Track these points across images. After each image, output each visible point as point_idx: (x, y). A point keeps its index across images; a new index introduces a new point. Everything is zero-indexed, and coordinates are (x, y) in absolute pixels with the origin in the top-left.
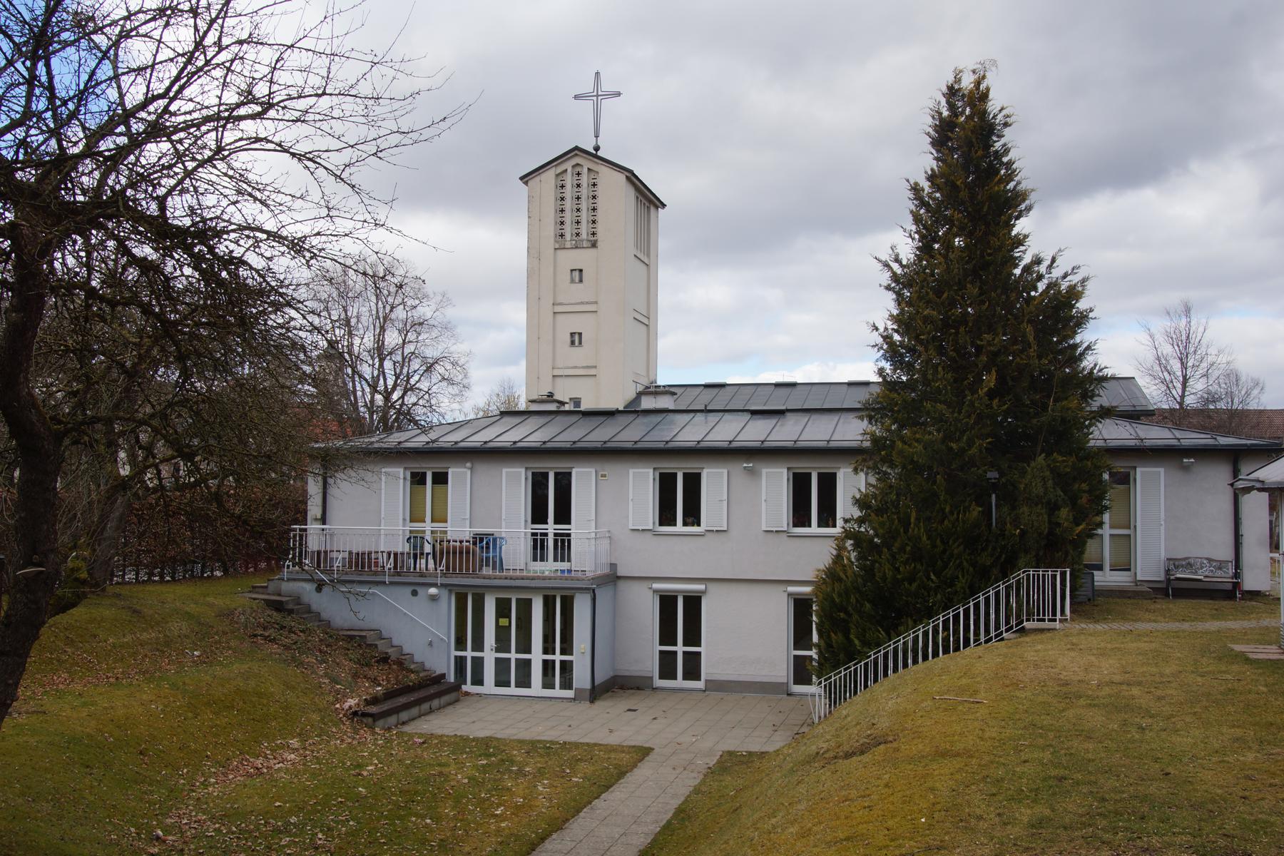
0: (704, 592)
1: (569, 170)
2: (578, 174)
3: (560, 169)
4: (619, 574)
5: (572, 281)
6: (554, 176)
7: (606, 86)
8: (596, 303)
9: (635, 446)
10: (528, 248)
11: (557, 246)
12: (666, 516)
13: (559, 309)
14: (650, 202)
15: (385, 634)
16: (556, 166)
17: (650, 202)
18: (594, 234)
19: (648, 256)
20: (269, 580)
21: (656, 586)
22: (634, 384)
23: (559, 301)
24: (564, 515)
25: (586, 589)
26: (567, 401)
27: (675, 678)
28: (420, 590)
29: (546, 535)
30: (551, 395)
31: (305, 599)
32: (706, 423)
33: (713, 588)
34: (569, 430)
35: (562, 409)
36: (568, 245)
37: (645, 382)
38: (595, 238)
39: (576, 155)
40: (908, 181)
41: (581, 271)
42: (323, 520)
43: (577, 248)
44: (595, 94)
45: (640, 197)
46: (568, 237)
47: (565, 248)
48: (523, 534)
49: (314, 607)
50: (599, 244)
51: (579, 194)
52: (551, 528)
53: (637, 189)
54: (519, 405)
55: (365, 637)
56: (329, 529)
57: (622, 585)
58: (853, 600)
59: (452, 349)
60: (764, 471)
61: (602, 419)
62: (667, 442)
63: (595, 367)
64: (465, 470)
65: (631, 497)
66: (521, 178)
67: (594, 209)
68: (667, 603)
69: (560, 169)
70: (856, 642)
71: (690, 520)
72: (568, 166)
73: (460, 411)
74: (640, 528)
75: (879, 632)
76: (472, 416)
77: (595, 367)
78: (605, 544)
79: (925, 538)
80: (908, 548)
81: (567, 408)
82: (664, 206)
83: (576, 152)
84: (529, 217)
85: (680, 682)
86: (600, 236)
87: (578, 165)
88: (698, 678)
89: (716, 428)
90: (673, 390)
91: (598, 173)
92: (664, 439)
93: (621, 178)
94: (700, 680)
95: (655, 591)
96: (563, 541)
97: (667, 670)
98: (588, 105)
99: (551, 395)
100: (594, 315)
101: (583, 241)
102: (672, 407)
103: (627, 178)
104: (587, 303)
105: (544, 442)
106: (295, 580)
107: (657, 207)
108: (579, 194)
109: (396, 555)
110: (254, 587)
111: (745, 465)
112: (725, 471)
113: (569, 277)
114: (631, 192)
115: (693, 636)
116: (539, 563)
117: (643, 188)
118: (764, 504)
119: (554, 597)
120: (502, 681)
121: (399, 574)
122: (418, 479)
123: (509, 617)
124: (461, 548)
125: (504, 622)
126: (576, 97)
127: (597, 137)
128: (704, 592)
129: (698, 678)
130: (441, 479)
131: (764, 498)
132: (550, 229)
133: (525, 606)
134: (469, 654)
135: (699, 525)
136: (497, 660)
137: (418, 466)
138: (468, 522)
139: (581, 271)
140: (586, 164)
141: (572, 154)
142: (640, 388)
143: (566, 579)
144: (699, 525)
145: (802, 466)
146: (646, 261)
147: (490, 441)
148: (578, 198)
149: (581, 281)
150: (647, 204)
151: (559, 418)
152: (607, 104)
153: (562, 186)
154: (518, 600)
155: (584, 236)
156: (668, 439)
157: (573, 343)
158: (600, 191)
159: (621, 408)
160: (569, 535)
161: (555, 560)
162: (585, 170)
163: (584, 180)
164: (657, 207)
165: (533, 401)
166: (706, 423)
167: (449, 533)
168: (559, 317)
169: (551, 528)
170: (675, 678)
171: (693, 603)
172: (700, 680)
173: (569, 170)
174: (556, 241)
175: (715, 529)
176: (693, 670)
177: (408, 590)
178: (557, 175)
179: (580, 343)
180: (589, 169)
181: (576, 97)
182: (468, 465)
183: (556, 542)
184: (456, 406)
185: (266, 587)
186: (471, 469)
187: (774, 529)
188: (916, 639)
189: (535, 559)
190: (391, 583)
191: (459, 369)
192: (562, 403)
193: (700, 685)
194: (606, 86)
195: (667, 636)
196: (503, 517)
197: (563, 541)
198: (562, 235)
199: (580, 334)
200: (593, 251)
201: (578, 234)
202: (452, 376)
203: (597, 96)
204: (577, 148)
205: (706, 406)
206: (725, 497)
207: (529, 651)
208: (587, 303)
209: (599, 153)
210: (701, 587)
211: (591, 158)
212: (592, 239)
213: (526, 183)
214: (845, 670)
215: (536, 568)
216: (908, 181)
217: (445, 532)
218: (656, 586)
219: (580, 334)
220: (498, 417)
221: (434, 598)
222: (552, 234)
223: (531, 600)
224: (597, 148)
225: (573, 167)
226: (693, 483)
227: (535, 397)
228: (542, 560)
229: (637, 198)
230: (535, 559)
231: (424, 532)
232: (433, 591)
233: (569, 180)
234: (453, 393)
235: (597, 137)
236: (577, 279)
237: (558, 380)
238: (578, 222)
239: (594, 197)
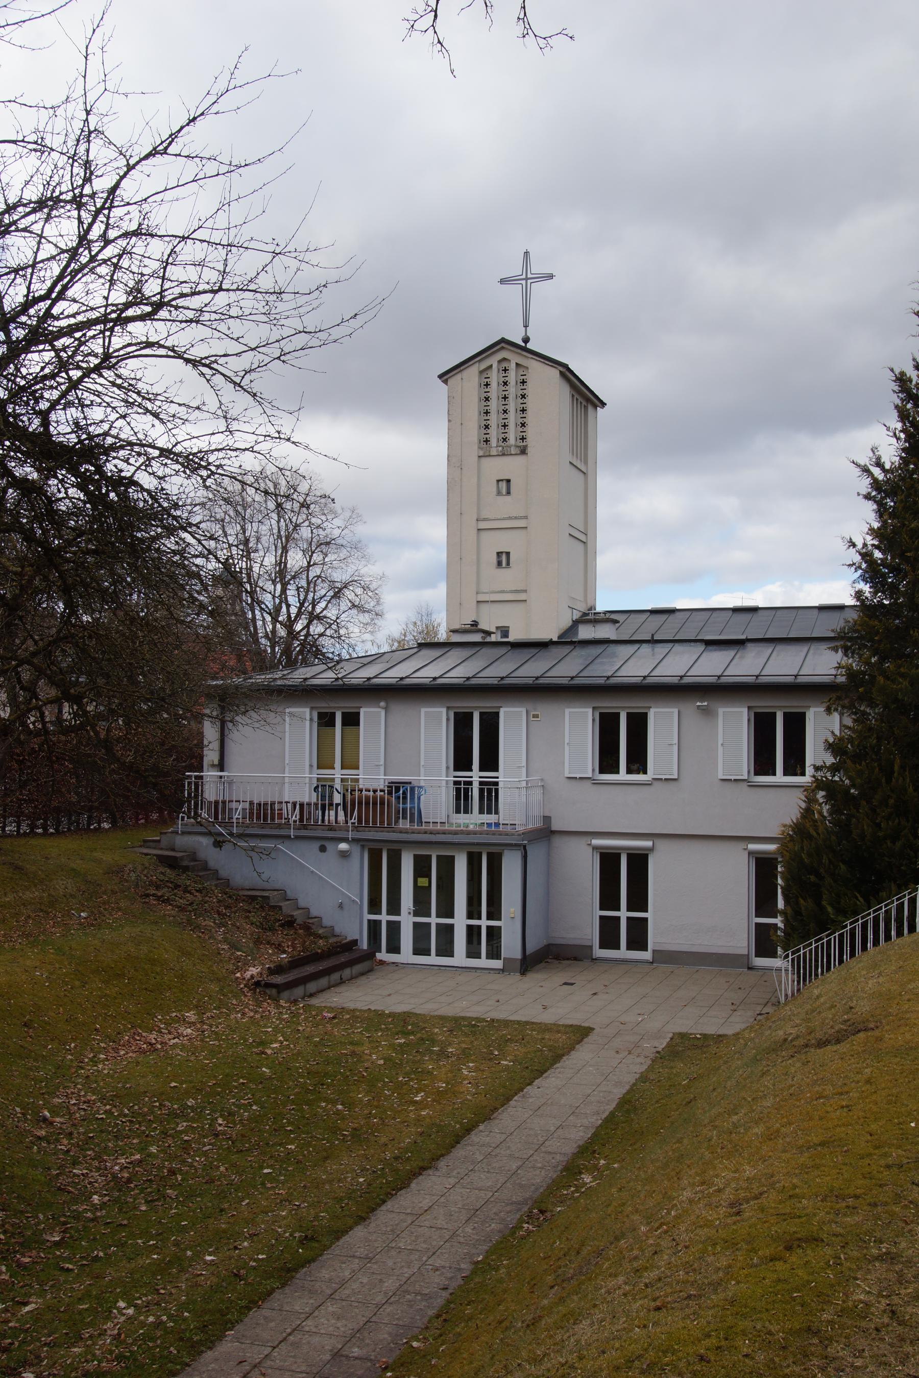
0: (652, 849)
1: (495, 366)
2: (505, 370)
3: (484, 365)
4: (553, 828)
5: (499, 493)
6: (477, 373)
7: (537, 268)
8: (526, 517)
9: (571, 682)
10: (448, 456)
11: (481, 453)
12: (608, 763)
13: (482, 525)
14: (588, 400)
15: (290, 894)
16: (480, 361)
17: (588, 400)
18: (523, 439)
19: (586, 463)
20: (161, 833)
21: (597, 842)
22: (570, 610)
23: (485, 514)
24: (490, 761)
25: (516, 845)
26: (494, 630)
27: (618, 947)
28: (330, 846)
29: (470, 783)
30: (475, 624)
31: (202, 855)
32: (653, 655)
33: (661, 845)
34: (494, 665)
35: (488, 639)
36: (494, 452)
37: (583, 608)
38: (524, 444)
39: (503, 348)
40: (892, 370)
41: (508, 481)
42: (221, 766)
43: (504, 455)
44: (524, 276)
45: (576, 396)
46: (494, 442)
47: (490, 456)
48: (444, 783)
49: (212, 864)
50: (529, 450)
51: (506, 393)
52: (476, 775)
53: (573, 386)
54: (439, 636)
55: (268, 898)
56: (228, 777)
57: (557, 841)
58: (825, 860)
59: (362, 572)
60: (721, 711)
61: (533, 651)
62: (608, 678)
63: (525, 591)
64: (379, 710)
65: (567, 741)
66: (440, 377)
67: (523, 410)
68: (609, 860)
69: (484, 365)
70: (830, 909)
71: (635, 767)
72: (493, 361)
73: (373, 642)
74: (578, 776)
75: (857, 898)
76: (385, 648)
77: (525, 591)
78: (537, 795)
79: (911, 789)
80: (891, 801)
81: (493, 638)
82: (603, 404)
83: (503, 345)
84: (449, 421)
85: (623, 953)
86: (531, 442)
87: (504, 359)
88: (644, 948)
89: (665, 660)
90: (613, 616)
91: (527, 368)
92: (605, 674)
93: (554, 373)
94: (647, 950)
95: (595, 848)
96: (490, 791)
97: (609, 938)
98: (515, 291)
99: (475, 624)
100: (524, 531)
101: (510, 447)
102: (613, 637)
103: (561, 373)
104: (516, 518)
105: (468, 678)
106: (190, 833)
107: (595, 407)
108: (506, 393)
109: (302, 805)
110: (145, 841)
111: (698, 704)
112: (676, 711)
113: (495, 489)
114: (566, 390)
115: (639, 900)
116: (462, 815)
117: (585, 390)
118: (720, 749)
119: (480, 854)
120: (421, 949)
121: (305, 827)
122: (326, 720)
123: (429, 876)
124: (382, 799)
125: (422, 882)
126: (502, 281)
127: (526, 326)
128: (652, 849)
129: (644, 948)
130: (352, 720)
131: (720, 742)
132: (473, 434)
133: (447, 865)
134: (384, 917)
135: (645, 772)
136: (452, 916)
137: (326, 705)
138: (382, 768)
139: (508, 481)
140: (514, 358)
141: (498, 347)
142: (577, 615)
143: (494, 834)
144: (645, 772)
145: (764, 704)
146: (583, 469)
147: (407, 677)
148: (505, 398)
149: (508, 493)
150: (584, 403)
151: (485, 651)
152: (538, 289)
153: (487, 385)
154: (438, 857)
155: (512, 441)
156: (610, 674)
157: (499, 564)
158: (531, 389)
159: (555, 639)
160: (496, 784)
161: (481, 812)
162: (513, 365)
163: (512, 377)
164: (595, 407)
165: (454, 631)
166: (653, 655)
167: (361, 781)
168: (483, 534)
169: (476, 775)
170: (618, 947)
171: (639, 862)
172: (647, 950)
173: (495, 366)
174: (479, 448)
175: (663, 777)
176: (638, 939)
177: (316, 845)
178: (481, 372)
179: (508, 564)
180: (517, 364)
181: (502, 281)
182: (382, 704)
183: (481, 791)
184: (367, 636)
185: (159, 841)
186: (386, 709)
187: (733, 778)
188: (900, 908)
189: (458, 811)
190: (297, 837)
191: (370, 594)
192: (488, 633)
193: (647, 955)
194: (537, 268)
195: (609, 899)
196: (422, 763)
197: (490, 791)
198: (487, 441)
199: (508, 554)
200: (521, 459)
201: (505, 440)
202: (363, 602)
203: (527, 279)
204: (503, 340)
205: (653, 635)
206: (676, 741)
207: (416, 925)
208: (516, 518)
209: (529, 346)
210: (648, 844)
211: (519, 351)
212: (521, 444)
213: (446, 382)
214: (816, 941)
215: (458, 821)
216: (892, 370)
217: (357, 780)
218: (597, 842)
219: (508, 554)
220: (416, 650)
221: (344, 855)
222: (476, 440)
223: (453, 857)
224: (526, 340)
225: (500, 362)
226: (638, 724)
227: (457, 626)
228: (466, 812)
229: (573, 396)
230: (458, 811)
231: (333, 780)
232: (343, 846)
233: (495, 377)
234: (365, 622)
235: (526, 326)
236: (504, 491)
237: (484, 607)
238: (505, 426)
239: (523, 396)
